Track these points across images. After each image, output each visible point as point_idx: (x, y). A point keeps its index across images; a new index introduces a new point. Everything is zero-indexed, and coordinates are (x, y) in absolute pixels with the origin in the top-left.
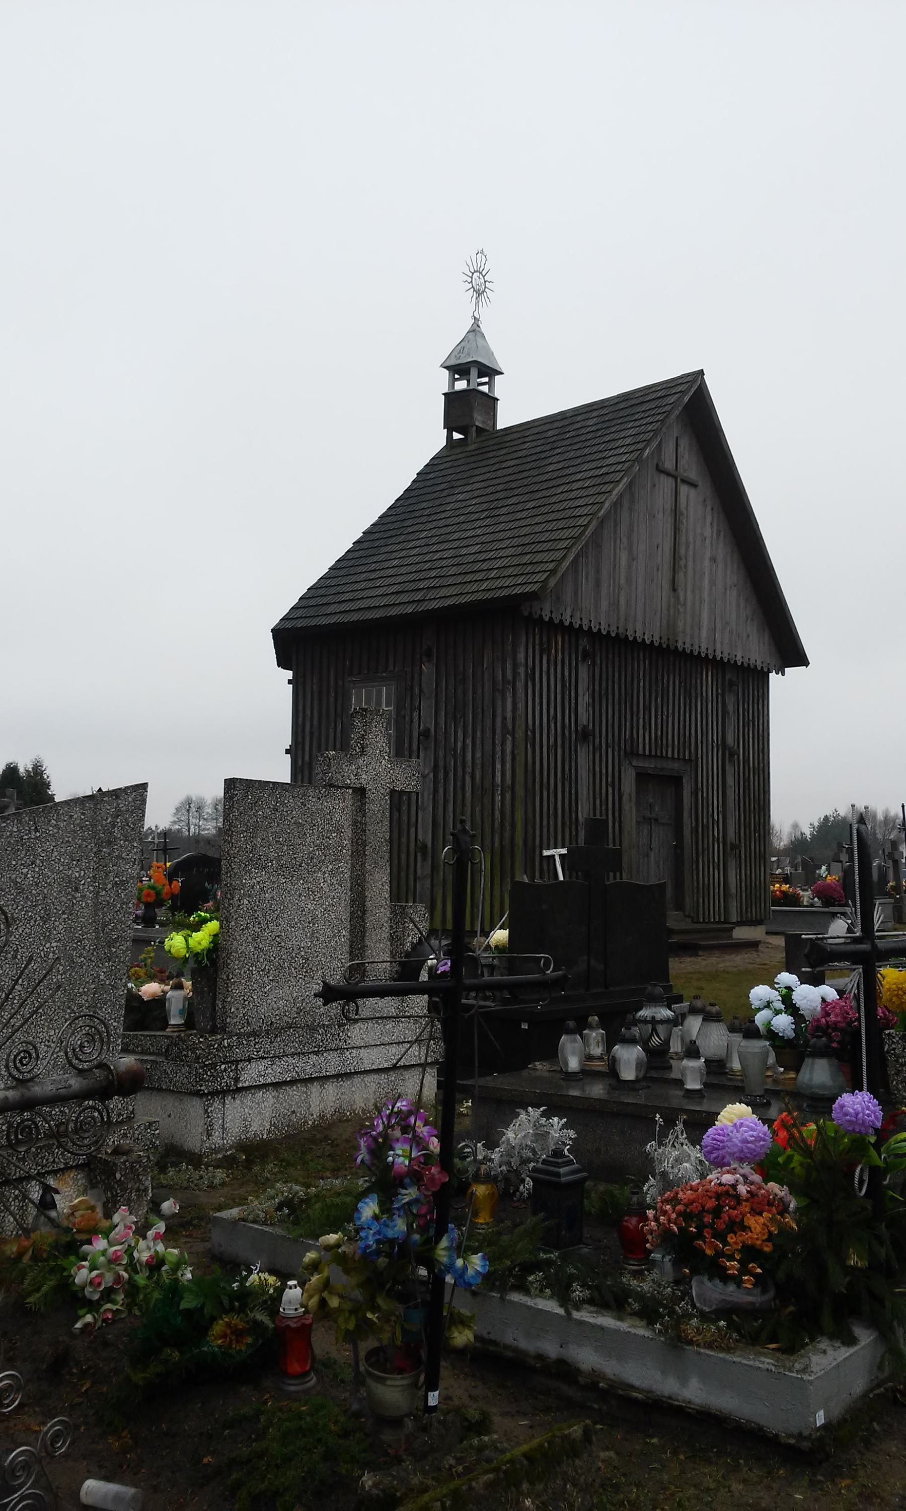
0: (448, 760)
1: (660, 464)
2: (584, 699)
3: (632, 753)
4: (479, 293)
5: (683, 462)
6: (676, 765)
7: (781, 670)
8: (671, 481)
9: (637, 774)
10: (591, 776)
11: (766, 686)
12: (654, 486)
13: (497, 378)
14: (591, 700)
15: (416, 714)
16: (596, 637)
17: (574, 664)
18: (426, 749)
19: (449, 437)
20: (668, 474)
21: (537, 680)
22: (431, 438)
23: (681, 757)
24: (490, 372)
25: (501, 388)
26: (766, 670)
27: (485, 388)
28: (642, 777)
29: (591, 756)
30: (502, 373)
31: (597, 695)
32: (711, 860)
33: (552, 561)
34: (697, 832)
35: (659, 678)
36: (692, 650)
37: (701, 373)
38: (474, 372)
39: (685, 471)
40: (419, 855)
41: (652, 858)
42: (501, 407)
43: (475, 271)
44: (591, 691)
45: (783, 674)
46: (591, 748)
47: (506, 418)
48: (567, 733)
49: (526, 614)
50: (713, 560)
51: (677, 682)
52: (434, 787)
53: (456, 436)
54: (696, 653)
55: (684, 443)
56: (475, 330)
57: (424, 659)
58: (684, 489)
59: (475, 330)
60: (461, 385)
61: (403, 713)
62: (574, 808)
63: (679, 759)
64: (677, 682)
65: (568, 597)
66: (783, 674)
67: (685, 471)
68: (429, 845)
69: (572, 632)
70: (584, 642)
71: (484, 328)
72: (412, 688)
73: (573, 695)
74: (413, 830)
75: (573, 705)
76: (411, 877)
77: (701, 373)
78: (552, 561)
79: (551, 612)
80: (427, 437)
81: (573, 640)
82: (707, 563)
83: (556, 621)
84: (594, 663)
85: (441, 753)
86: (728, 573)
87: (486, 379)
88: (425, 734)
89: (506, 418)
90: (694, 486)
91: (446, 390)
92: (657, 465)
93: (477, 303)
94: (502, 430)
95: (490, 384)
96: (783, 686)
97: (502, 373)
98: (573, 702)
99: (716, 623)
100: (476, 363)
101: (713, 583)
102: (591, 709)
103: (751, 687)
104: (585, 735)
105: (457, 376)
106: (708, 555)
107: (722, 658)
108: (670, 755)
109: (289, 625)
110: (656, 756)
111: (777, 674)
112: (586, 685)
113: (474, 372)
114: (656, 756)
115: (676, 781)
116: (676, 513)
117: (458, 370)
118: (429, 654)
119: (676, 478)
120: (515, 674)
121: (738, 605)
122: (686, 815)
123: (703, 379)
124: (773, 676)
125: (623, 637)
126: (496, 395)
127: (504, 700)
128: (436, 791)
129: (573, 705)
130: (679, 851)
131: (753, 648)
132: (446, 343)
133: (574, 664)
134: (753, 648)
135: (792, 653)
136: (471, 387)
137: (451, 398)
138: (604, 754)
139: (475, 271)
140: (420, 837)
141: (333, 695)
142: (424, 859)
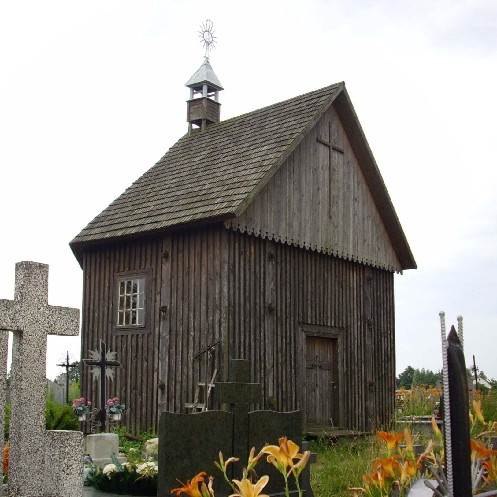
0: (178, 327)
1: (319, 138)
2: (270, 286)
3: (305, 323)
4: (208, 43)
5: (334, 138)
6: (333, 331)
7: (400, 271)
8: (327, 150)
9: (307, 337)
10: (275, 337)
11: (391, 277)
12: (316, 151)
13: (220, 93)
14: (275, 288)
15: (158, 297)
16: (277, 245)
17: (262, 263)
18: (164, 318)
19: (191, 128)
20: (325, 144)
21: (237, 272)
22: (179, 128)
23: (337, 326)
24: (214, 88)
25: (222, 98)
26: (391, 271)
27: (213, 98)
28: (310, 338)
29: (275, 325)
30: (222, 89)
31: (279, 283)
32: (357, 392)
33: (246, 193)
34: (347, 375)
35: (322, 274)
36: (342, 257)
37: (343, 83)
38: (205, 88)
39: (335, 143)
40: (160, 390)
41: (318, 392)
42: (222, 110)
43: (206, 31)
44: (274, 281)
45: (402, 274)
46: (275, 318)
47: (225, 115)
48: (258, 309)
49: (228, 228)
50: (355, 199)
51: (334, 278)
52: (170, 345)
53: (195, 127)
54: (345, 258)
55: (334, 127)
56: (207, 64)
57: (164, 260)
58: (335, 155)
59: (207, 64)
60: (198, 96)
61: (150, 296)
62: (263, 358)
63: (335, 327)
64: (334, 278)
65: (258, 220)
66: (402, 274)
67: (335, 143)
68: (166, 384)
69: (260, 241)
70: (270, 250)
71: (211, 63)
72: (156, 279)
73: (262, 283)
74: (156, 374)
75: (262, 290)
76: (155, 405)
77: (343, 83)
78: (246, 193)
79: (246, 227)
80: (177, 127)
81: (262, 247)
82: (351, 202)
83: (250, 234)
84: (277, 263)
85: (173, 323)
86: (366, 208)
87: (213, 93)
88: (163, 309)
89: (225, 115)
90: (341, 152)
91: (188, 99)
92: (317, 138)
93: (207, 49)
94: (222, 122)
95: (216, 96)
96: (402, 281)
97: (222, 89)
98: (262, 288)
99: (361, 244)
100: (206, 82)
101: (355, 214)
102: (274, 293)
103: (382, 280)
104: (271, 310)
105: (195, 91)
106: (352, 197)
107: (362, 262)
108: (329, 324)
109: (79, 239)
110: (316, 325)
111: (398, 273)
112: (271, 276)
113: (205, 88)
114: (320, 325)
115: (334, 341)
116: (331, 169)
117: (196, 87)
118: (166, 256)
119: (329, 147)
120: (221, 268)
121: (372, 231)
122: (340, 365)
123: (344, 87)
124: (395, 274)
125: (296, 246)
126: (219, 102)
127: (214, 284)
128: (170, 347)
129: (262, 290)
130: (335, 387)
131: (383, 258)
132: (190, 72)
133: (262, 263)
134: (383, 258)
135: (406, 261)
136: (204, 96)
137: (191, 103)
138: (284, 323)
139: (206, 31)
140: (160, 378)
141: (107, 285)
142: (163, 393)
